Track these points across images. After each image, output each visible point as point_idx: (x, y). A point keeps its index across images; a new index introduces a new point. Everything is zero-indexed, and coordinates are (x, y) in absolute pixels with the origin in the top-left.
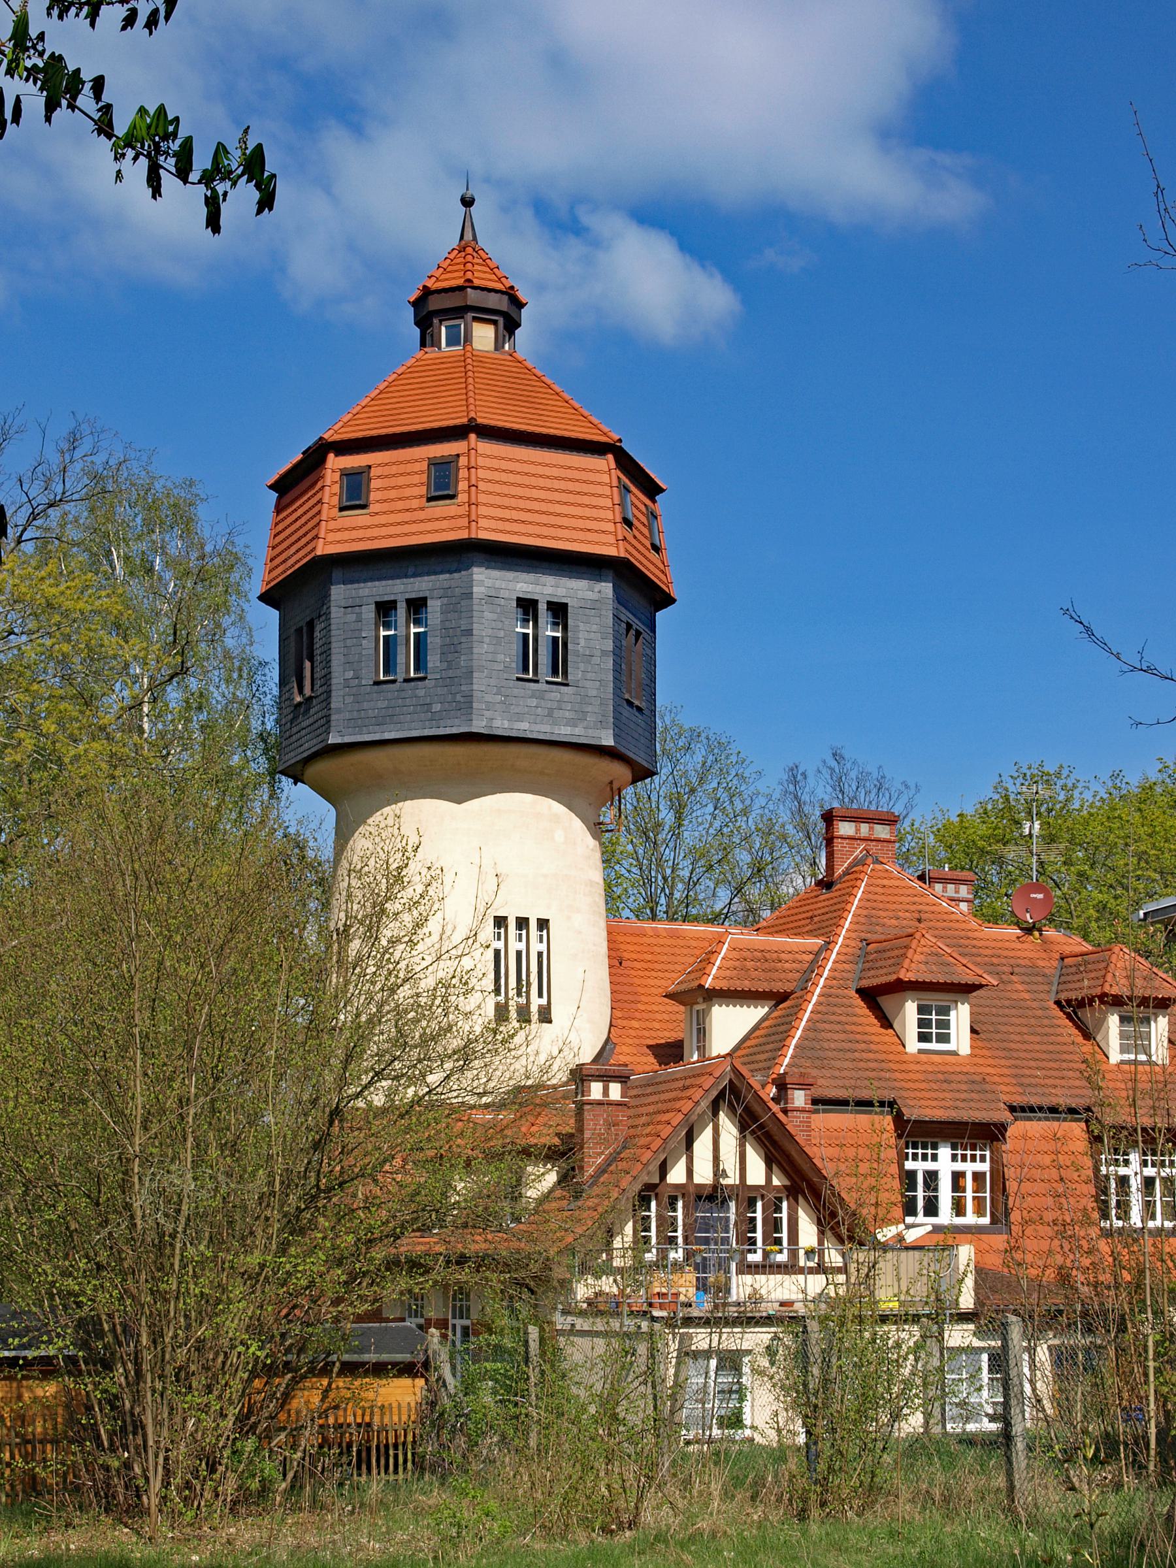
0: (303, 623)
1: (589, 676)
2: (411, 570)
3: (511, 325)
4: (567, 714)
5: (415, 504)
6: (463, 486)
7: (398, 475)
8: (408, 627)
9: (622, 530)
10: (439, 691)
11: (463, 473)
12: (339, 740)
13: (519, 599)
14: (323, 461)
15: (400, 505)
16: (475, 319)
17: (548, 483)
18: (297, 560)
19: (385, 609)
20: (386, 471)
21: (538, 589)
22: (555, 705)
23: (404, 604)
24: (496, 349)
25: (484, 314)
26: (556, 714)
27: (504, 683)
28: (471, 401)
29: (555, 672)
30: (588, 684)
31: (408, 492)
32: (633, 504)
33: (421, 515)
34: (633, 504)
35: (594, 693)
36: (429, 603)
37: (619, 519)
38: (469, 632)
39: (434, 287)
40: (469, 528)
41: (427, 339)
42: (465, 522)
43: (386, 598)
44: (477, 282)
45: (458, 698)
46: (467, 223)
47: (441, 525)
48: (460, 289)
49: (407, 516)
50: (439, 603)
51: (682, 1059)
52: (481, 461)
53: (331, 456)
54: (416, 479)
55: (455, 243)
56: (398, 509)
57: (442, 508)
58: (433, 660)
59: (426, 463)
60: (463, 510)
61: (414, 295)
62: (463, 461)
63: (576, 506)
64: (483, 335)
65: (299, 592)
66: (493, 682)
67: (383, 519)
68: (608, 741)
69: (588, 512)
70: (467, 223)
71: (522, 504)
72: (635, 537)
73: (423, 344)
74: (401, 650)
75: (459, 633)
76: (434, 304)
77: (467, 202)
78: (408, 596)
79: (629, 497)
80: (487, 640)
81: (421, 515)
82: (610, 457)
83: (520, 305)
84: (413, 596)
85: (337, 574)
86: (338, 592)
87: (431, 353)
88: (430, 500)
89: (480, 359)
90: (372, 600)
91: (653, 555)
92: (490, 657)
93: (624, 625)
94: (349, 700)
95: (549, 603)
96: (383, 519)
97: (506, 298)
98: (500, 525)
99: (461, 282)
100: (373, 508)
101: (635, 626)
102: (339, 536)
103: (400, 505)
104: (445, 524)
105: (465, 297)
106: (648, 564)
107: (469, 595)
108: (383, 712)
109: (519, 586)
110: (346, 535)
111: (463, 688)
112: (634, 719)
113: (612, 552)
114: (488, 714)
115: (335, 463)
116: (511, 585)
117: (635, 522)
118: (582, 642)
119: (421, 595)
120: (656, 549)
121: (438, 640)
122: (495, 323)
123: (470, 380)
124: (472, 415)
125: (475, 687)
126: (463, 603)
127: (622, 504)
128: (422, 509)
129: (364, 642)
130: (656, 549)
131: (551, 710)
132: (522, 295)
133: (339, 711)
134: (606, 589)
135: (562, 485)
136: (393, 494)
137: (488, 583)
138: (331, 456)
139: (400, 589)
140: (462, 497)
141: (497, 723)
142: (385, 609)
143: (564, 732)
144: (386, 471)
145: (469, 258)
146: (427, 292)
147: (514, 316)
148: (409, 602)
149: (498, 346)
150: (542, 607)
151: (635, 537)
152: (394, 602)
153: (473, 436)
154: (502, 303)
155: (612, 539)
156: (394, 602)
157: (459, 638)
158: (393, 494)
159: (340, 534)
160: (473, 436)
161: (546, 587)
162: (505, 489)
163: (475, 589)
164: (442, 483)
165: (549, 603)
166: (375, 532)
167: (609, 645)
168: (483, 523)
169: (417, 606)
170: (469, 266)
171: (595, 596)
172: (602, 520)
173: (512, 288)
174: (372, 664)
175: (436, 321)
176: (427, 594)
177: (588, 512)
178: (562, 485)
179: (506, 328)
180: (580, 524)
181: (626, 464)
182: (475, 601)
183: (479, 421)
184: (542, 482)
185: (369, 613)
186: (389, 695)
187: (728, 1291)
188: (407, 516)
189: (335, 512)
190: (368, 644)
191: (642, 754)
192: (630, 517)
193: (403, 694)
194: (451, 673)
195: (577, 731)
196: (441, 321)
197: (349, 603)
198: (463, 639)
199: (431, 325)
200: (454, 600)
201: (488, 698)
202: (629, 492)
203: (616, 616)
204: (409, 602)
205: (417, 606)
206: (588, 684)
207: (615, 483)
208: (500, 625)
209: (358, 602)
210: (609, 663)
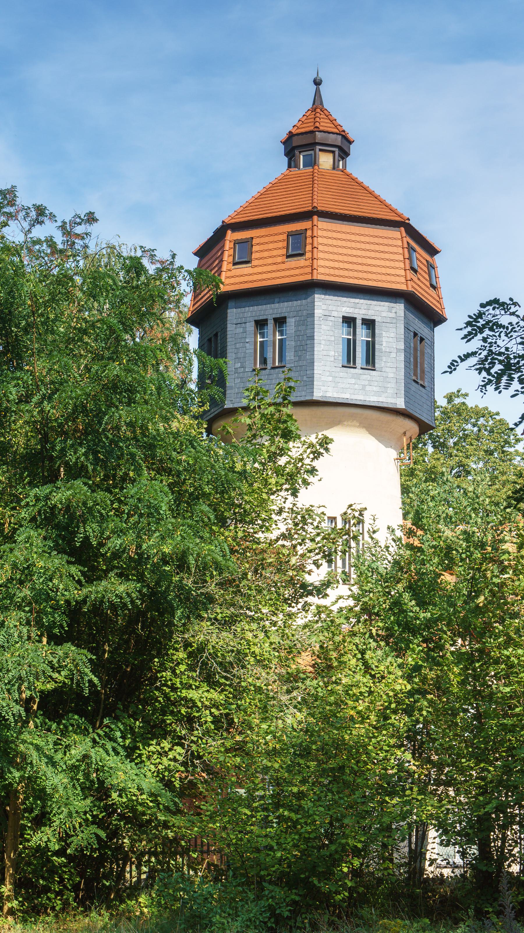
0: (212, 335)
1: (389, 365)
2: (277, 300)
3: (344, 154)
4: (375, 389)
5: (279, 259)
6: (309, 248)
7: (269, 244)
8: (274, 335)
9: (410, 274)
11: (309, 240)
12: (231, 406)
13: (344, 317)
14: (224, 235)
15: (270, 261)
16: (321, 150)
17: (363, 246)
18: (207, 294)
19: (261, 324)
21: (357, 311)
22: (367, 383)
23: (272, 321)
24: (334, 168)
25: (327, 147)
26: (368, 388)
27: (334, 369)
28: (315, 197)
29: (368, 362)
30: (388, 370)
31: (275, 253)
32: (417, 259)
33: (283, 266)
34: (417, 259)
35: (392, 375)
36: (288, 320)
37: (408, 267)
40: (312, 273)
41: (292, 163)
42: (309, 270)
43: (261, 318)
44: (321, 128)
45: (305, 378)
46: (318, 95)
47: (293, 272)
48: (312, 132)
49: (274, 268)
50: (293, 320)
52: (320, 233)
53: (229, 232)
54: (280, 245)
55: (310, 106)
56: (268, 263)
57: (294, 262)
58: (290, 355)
59: (285, 235)
60: (308, 263)
61: (284, 136)
62: (309, 233)
63: (381, 259)
64: (325, 160)
65: (210, 316)
66: (327, 368)
67: (259, 270)
68: (401, 404)
69: (388, 263)
70: (318, 95)
71: (346, 259)
72: (419, 279)
73: (290, 166)
74: (270, 350)
75: (305, 338)
76: (296, 142)
78: (274, 316)
79: (414, 255)
80: (323, 342)
81: (283, 266)
82: (402, 229)
83: (350, 142)
84: (278, 316)
85: (231, 304)
86: (233, 314)
87: (294, 171)
88: (288, 257)
89: (322, 174)
90: (252, 319)
91: (431, 291)
92: (325, 353)
93: (412, 334)
94: (238, 381)
95: (363, 320)
96: (259, 270)
97: (339, 137)
98: (332, 272)
99: (312, 128)
100: (254, 263)
101: (419, 335)
102: (232, 280)
103: (270, 261)
104: (297, 272)
105: (315, 137)
106: (427, 296)
107: (312, 315)
109: (344, 309)
110: (237, 280)
111: (308, 372)
112: (419, 392)
113: (403, 287)
114: (323, 388)
115: (230, 236)
116: (339, 309)
117: (419, 270)
118: (384, 344)
119: (283, 315)
120: (434, 287)
121: (293, 343)
122: (333, 152)
123: (316, 185)
124: (315, 205)
125: (315, 372)
126: (309, 320)
127: (410, 258)
128: (283, 263)
129: (247, 345)
130: (434, 287)
131: (364, 386)
132: (351, 136)
133: (231, 388)
134: (399, 308)
135: (372, 247)
136: (266, 254)
137: (324, 307)
138: (229, 232)
139: (270, 310)
140: (308, 255)
141: (329, 394)
142: (261, 324)
143: (373, 399)
145: (318, 115)
147: (345, 148)
148: (276, 320)
149: (335, 167)
150: (359, 322)
151: (419, 279)
152: (266, 320)
153: (315, 218)
154: (338, 140)
155: (403, 280)
156: (266, 320)
157: (306, 342)
158: (266, 254)
159: (233, 277)
161: (361, 308)
162: (335, 250)
163: (316, 311)
164: (297, 246)
165: (363, 320)
166: (255, 277)
167: (402, 346)
168: (321, 270)
169: (280, 322)
170: (318, 119)
171: (393, 315)
172: (397, 268)
173: (344, 131)
174: (252, 358)
175: (297, 152)
176: (286, 315)
177: (388, 263)
178: (372, 247)
179: (340, 156)
180: (384, 270)
181: (413, 233)
182: (316, 319)
183: (319, 208)
184: (358, 245)
185: (251, 327)
188: (274, 268)
189: (231, 266)
190: (250, 347)
191: (425, 415)
192: (416, 267)
193: (271, 377)
194: (301, 363)
195: (381, 399)
196: (300, 152)
197: (239, 321)
198: (308, 342)
199: (294, 156)
200: (302, 318)
201: (324, 378)
202: (415, 251)
203: (406, 328)
204: (276, 320)
205: (280, 322)
206: (388, 370)
207: (406, 245)
208: (331, 333)
209: (243, 320)
210: (402, 357)
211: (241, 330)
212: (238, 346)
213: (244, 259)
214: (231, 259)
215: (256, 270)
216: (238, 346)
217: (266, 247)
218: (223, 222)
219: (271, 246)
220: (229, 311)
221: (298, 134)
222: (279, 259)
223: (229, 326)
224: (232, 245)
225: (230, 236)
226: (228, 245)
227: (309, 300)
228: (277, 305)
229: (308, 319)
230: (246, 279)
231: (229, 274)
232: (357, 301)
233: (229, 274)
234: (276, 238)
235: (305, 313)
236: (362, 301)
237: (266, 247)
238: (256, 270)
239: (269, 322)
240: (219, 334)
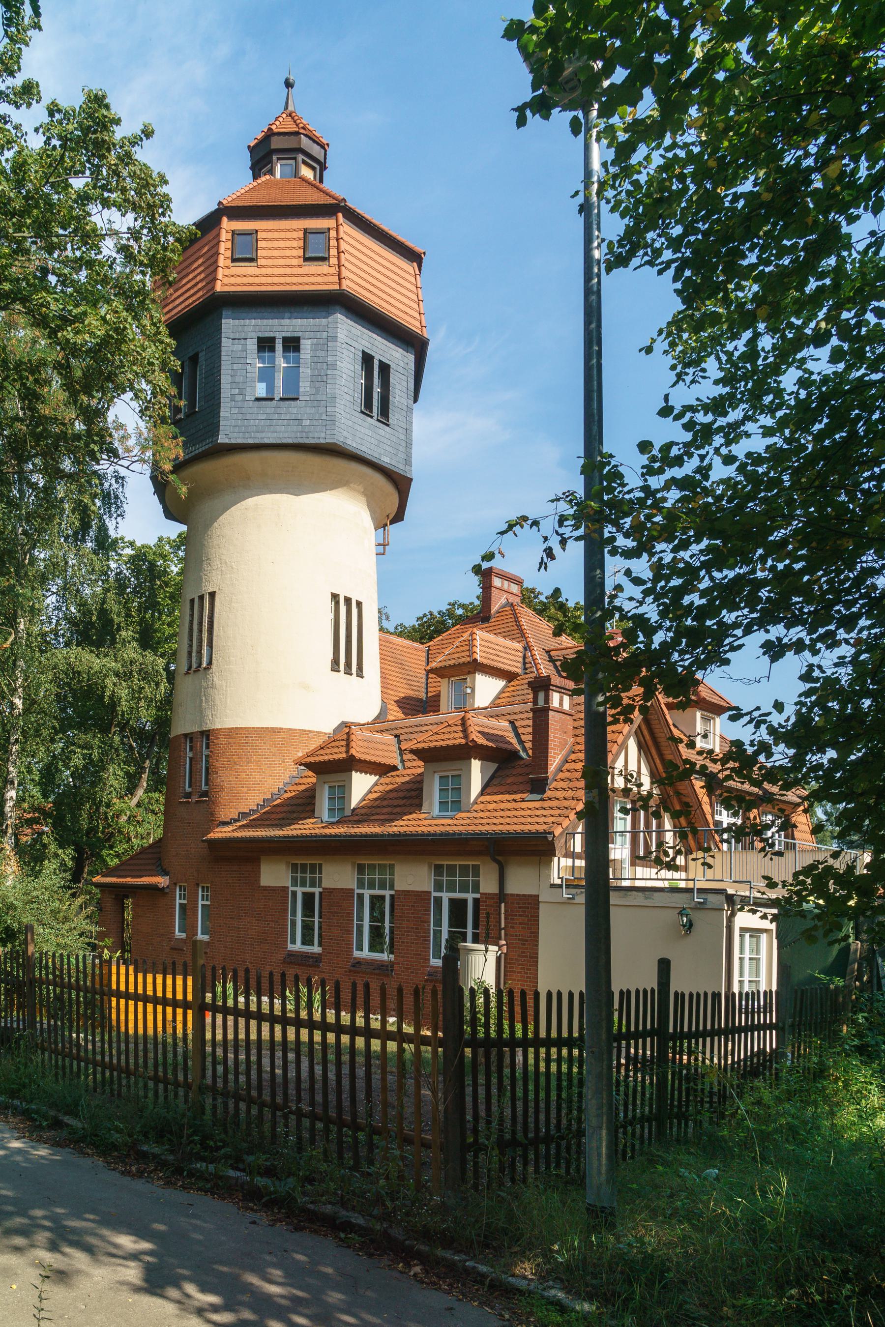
5: (295, 262)
6: (333, 252)
10: (308, 410)
14: (218, 222)
15: (282, 262)
16: (304, 162)
19: (266, 345)
20: (270, 235)
31: (288, 253)
38: (334, 366)
39: (275, 131)
43: (267, 335)
47: (316, 278)
49: (288, 271)
50: (309, 342)
51: (420, 806)
53: (225, 219)
54: (295, 244)
62: (333, 234)
67: (269, 271)
75: (325, 367)
77: (289, 84)
84: (289, 335)
86: (229, 325)
90: (255, 335)
103: (282, 262)
104: (319, 279)
108: (262, 423)
115: (227, 225)
119: (296, 335)
121: (308, 371)
128: (300, 266)
138: (225, 219)
139: (281, 326)
140: (333, 261)
141: (349, 442)
144: (270, 235)
146: (270, 134)
148: (286, 340)
157: (323, 373)
160: (340, 215)
166: (263, 280)
169: (292, 344)
175: (274, 158)
186: (268, 410)
187: (717, 658)
188: (288, 271)
193: (279, 410)
194: (319, 397)
196: (278, 159)
197: (237, 335)
200: (321, 342)
204: (286, 340)
209: (243, 336)
211: (240, 347)
212: (235, 367)
213: (245, 255)
214: (229, 254)
215: (263, 271)
216: (235, 367)
217: (275, 244)
218: (220, 203)
219: (282, 244)
220: (223, 321)
221: (279, 134)
222: (295, 262)
223: (223, 340)
224: (229, 236)
225: (227, 225)
226: (224, 236)
227: (331, 319)
228: (287, 321)
229: (327, 342)
230: (251, 280)
231: (227, 272)
232: (375, 336)
233: (227, 272)
234: (289, 235)
235: (325, 334)
236: (379, 338)
237: (275, 244)
238: (263, 271)
239: (277, 341)
240: (202, 356)
